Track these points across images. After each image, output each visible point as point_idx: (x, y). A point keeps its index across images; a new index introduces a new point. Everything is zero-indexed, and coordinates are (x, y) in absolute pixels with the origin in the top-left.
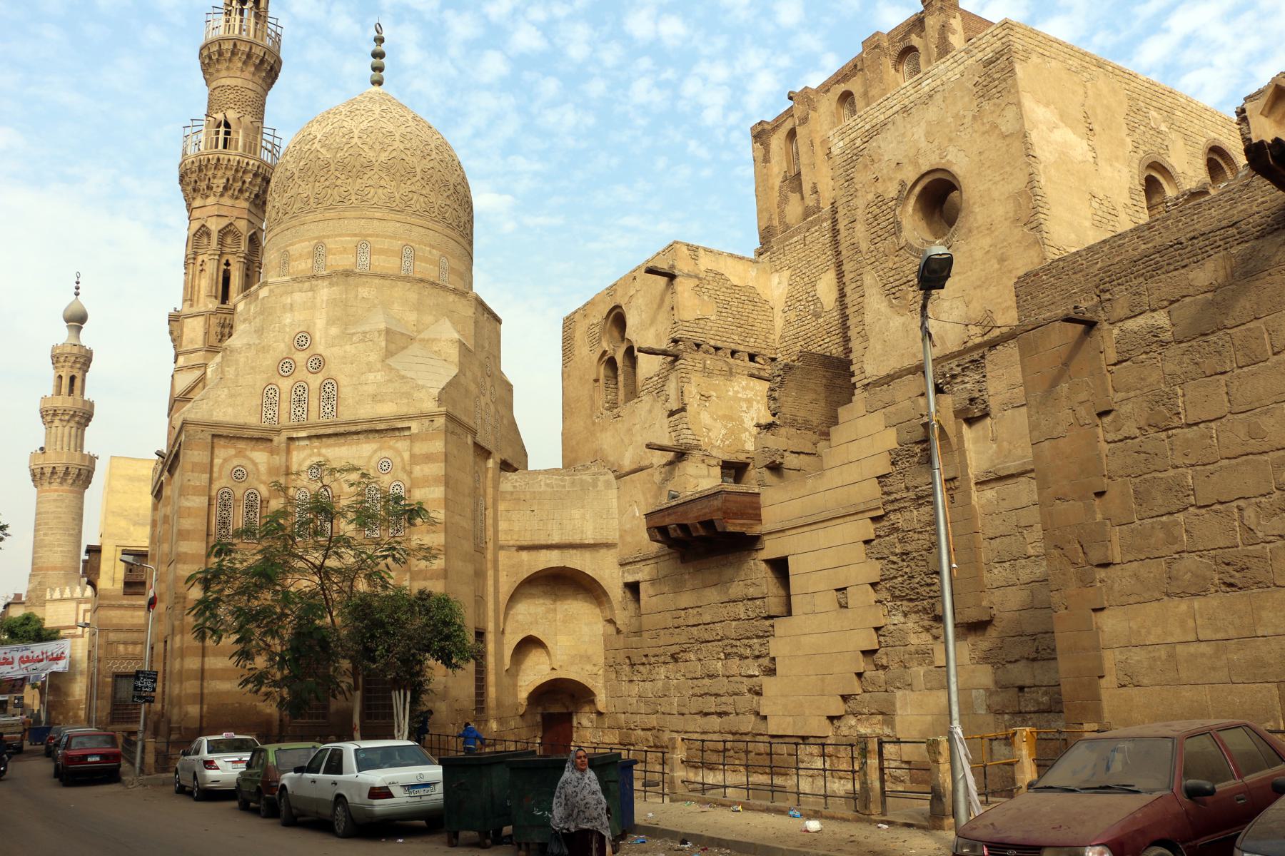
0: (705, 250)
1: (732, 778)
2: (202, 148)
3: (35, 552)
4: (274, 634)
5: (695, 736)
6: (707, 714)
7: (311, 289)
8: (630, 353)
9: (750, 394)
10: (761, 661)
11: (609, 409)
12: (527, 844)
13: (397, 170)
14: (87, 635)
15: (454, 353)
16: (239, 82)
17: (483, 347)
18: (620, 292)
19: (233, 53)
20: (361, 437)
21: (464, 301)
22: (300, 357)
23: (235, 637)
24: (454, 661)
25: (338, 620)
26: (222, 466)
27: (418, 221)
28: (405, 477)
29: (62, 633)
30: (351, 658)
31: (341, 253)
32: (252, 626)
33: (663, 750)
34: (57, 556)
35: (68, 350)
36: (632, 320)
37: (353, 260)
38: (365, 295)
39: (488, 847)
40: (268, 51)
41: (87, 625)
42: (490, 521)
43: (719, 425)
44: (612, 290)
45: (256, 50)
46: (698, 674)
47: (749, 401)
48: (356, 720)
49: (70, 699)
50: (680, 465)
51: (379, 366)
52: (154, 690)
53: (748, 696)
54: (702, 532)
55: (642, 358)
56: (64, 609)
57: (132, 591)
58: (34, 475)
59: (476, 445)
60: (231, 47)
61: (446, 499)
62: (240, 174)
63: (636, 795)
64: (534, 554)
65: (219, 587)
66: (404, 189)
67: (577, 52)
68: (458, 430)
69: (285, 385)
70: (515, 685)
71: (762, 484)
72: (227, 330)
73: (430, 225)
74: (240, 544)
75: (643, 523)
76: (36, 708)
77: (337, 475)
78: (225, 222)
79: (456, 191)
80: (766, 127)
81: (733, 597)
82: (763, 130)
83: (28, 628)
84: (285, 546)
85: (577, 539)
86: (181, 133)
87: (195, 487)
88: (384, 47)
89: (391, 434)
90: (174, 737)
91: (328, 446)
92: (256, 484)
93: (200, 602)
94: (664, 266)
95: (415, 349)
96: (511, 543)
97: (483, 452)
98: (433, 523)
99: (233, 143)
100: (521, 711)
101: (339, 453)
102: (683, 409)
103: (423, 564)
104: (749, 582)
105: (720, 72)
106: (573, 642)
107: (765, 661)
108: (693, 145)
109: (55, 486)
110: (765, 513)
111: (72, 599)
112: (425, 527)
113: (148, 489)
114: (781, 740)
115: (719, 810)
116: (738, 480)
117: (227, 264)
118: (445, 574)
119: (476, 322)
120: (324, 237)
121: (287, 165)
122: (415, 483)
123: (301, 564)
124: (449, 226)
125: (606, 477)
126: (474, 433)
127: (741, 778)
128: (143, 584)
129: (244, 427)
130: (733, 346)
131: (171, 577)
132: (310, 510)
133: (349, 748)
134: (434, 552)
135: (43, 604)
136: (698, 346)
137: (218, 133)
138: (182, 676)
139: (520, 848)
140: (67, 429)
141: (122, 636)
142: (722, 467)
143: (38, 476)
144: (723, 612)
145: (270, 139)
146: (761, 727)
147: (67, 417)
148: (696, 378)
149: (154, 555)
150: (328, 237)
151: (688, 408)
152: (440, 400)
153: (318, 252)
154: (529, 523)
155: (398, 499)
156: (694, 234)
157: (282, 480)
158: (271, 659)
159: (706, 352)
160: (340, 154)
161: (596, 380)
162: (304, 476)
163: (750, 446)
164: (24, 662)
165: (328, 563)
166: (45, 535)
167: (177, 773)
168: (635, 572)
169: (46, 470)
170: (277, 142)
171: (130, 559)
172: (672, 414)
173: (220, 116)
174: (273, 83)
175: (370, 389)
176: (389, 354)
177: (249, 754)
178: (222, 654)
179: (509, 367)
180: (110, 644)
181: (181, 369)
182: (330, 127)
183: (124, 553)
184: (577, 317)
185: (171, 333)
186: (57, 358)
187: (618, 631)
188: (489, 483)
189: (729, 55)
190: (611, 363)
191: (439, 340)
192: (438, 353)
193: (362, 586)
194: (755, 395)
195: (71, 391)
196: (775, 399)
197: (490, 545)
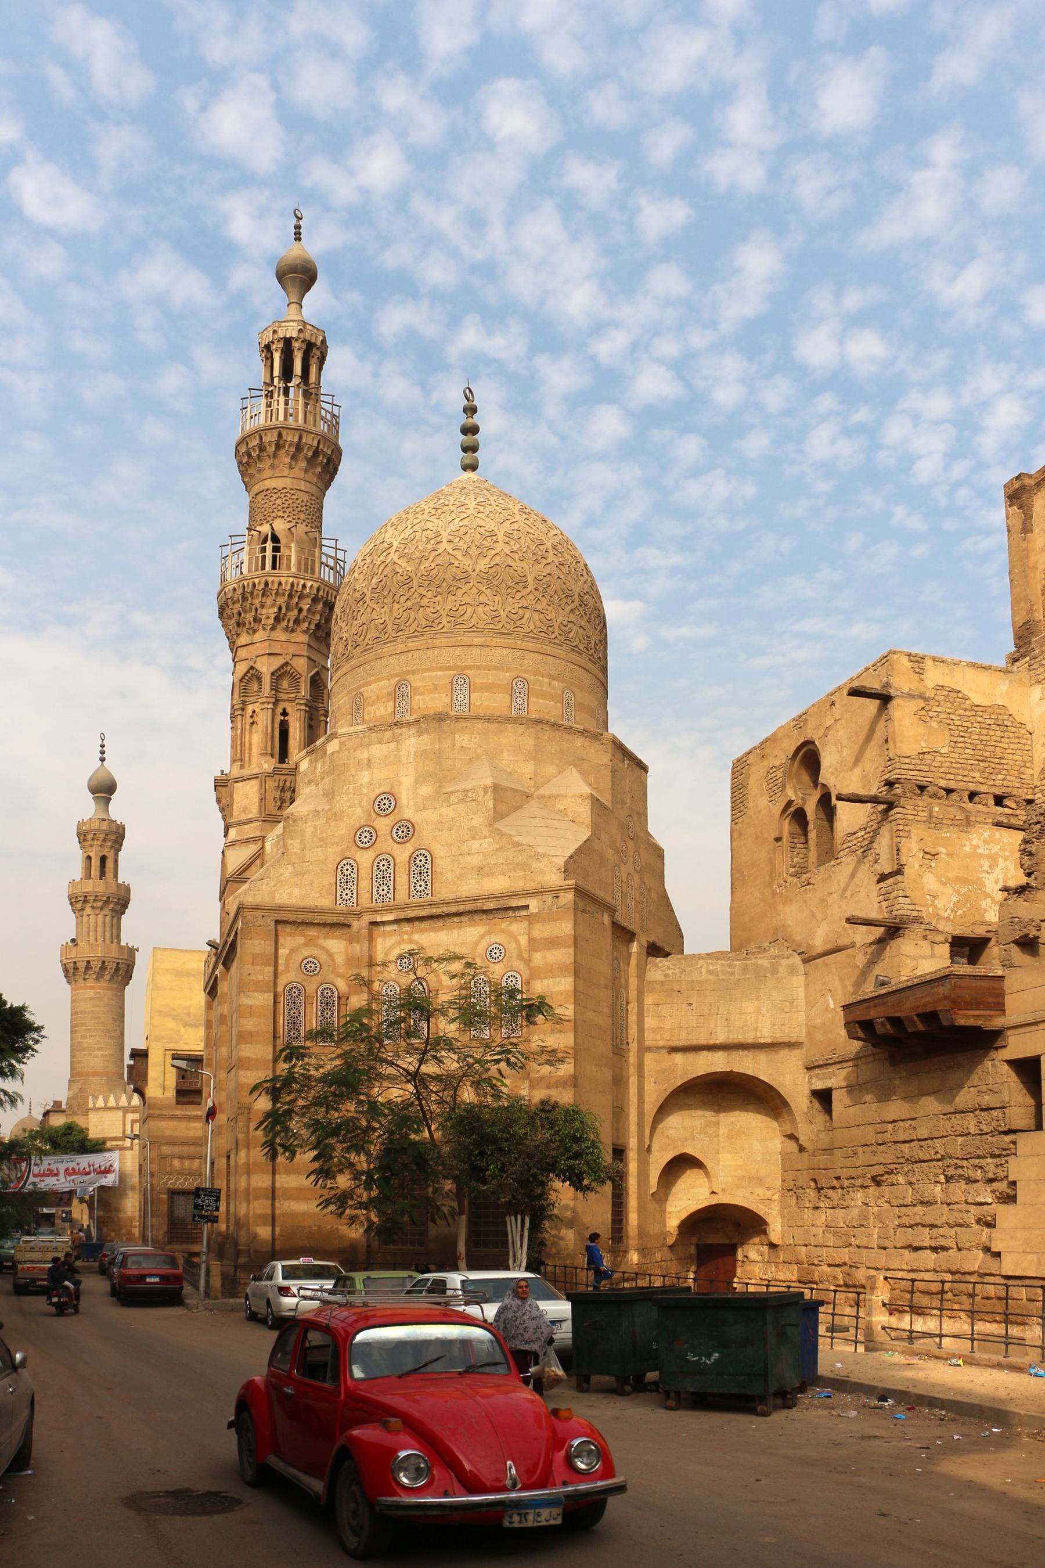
0: (934, 660)
1: (949, 1326)
2: (245, 571)
3: (72, 1056)
4: (359, 1149)
5: (900, 1275)
6: (917, 1249)
7: (394, 740)
8: (826, 803)
9: (995, 849)
10: (995, 1185)
11: (795, 875)
12: (678, 1393)
13: (502, 581)
14: (136, 1148)
15: (584, 812)
16: (287, 483)
17: (623, 803)
18: (812, 722)
19: (278, 447)
20: (464, 919)
21: (596, 745)
22: (383, 825)
23: (313, 1154)
24: (585, 1182)
25: (438, 1135)
26: (288, 958)
27: (532, 646)
28: (522, 966)
29: (109, 1145)
30: (456, 1179)
31: (430, 692)
32: (332, 1141)
33: (858, 1292)
34: (97, 1060)
35: (96, 826)
36: (828, 759)
37: (448, 700)
39: (628, 1394)
40: (323, 438)
41: (137, 1136)
42: (633, 1018)
43: (949, 890)
44: (800, 721)
45: (308, 440)
46: (908, 1201)
47: (993, 859)
48: (462, 1248)
49: (121, 1215)
50: (893, 943)
51: (486, 831)
52: (217, 1209)
53: (976, 1227)
54: (921, 1027)
55: (841, 807)
56: (108, 1119)
57: (185, 1100)
58: (66, 970)
59: (615, 925)
60: (296, 439)
61: (576, 991)
62: (295, 600)
63: (820, 1340)
64: (691, 1056)
65: (291, 1097)
66: (512, 605)
67: (727, 396)
68: (591, 908)
69: (365, 858)
70: (663, 1212)
71: (1007, 964)
72: (288, 795)
73: (549, 649)
74: (315, 1047)
75: (840, 1016)
76: (86, 1223)
77: (435, 965)
78: (278, 662)
79: (582, 603)
80: (1027, 482)
81: (960, 1107)
82: (1023, 487)
83: (71, 1138)
84: (370, 1050)
85: (749, 1038)
86: (217, 553)
87: (257, 982)
88: (477, 419)
89: (502, 914)
90: (242, 1260)
91: (422, 931)
92: (331, 977)
93: (268, 1115)
94: (876, 685)
95: (532, 808)
96: (661, 1043)
97: (624, 934)
98: (560, 1020)
99: (284, 562)
100: (670, 1241)
101: (436, 939)
102: (899, 872)
103: (546, 1069)
104: (984, 1088)
105: (939, 405)
106: (739, 1161)
107: (1003, 1186)
108: (900, 512)
109: (91, 982)
110: (1009, 1002)
111: (117, 1108)
112: (547, 1026)
113: (201, 985)
114: (1019, 1282)
115: (931, 1364)
116: (973, 960)
117: (285, 713)
118: (574, 1081)
119: (614, 772)
120: (408, 672)
121: (357, 583)
122: (535, 973)
123: (391, 1070)
124: (574, 649)
125: (790, 961)
126: (612, 911)
127: (963, 1326)
128: (199, 1092)
129: (313, 911)
130: (972, 787)
131: (232, 1085)
132: (401, 1007)
133: (455, 1279)
134: (560, 1055)
135: (86, 1112)
136: (922, 788)
137: (264, 550)
138: (249, 1195)
139: (668, 1397)
140: (100, 917)
141: (176, 1149)
142: (952, 945)
143: (71, 972)
144: (946, 1126)
145: (332, 552)
146: (992, 1266)
147: (99, 904)
148: (917, 831)
149: (209, 1060)
150: (413, 672)
151: (906, 870)
152: (566, 871)
153: (397, 695)
154: (677, 1020)
155: (512, 993)
156: (905, 636)
157: (365, 973)
158: (356, 1178)
159: (934, 796)
160: (425, 564)
161: (778, 839)
162: (392, 967)
163: (992, 916)
164: (70, 1175)
165: (425, 1069)
166: (83, 1037)
167: (247, 1298)
168: (825, 1077)
169: (79, 965)
170: (340, 555)
171: (183, 1064)
172: (883, 878)
173: (265, 529)
174: (332, 479)
175: (475, 861)
176: (498, 815)
177: (333, 1282)
178: (298, 1172)
179: (660, 825)
180: (163, 1158)
181: (233, 844)
182: (409, 531)
183: (175, 1057)
184: (751, 758)
185: (219, 801)
186: (83, 836)
187: (802, 1149)
188: (632, 971)
189: (952, 379)
190: (799, 817)
191: (565, 797)
192: (563, 812)
193: (468, 1095)
194: (1003, 849)
195: (103, 874)
196: (1031, 854)
197: (633, 1047)
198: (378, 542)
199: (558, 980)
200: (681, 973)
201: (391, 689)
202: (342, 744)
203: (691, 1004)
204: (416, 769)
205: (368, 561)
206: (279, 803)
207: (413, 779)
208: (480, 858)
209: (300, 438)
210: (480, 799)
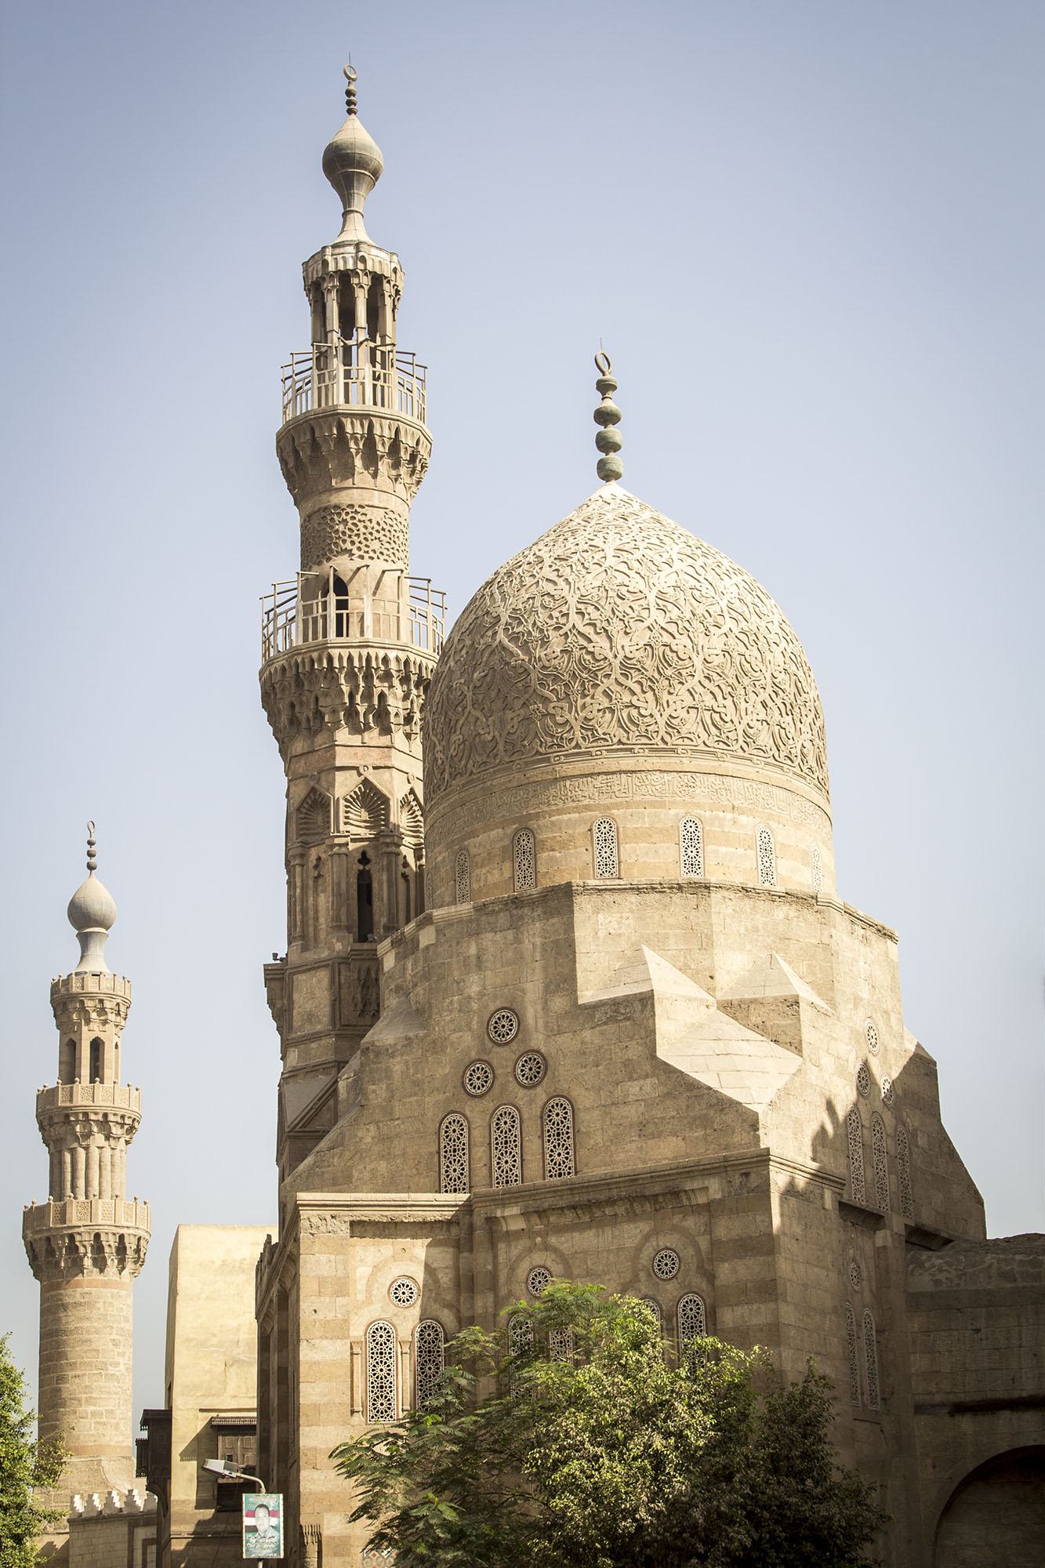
22: (503, 1058)
26: (371, 1281)
38: (613, 927)
64: (985, 1421)
69: (477, 1113)
96: (938, 1398)
99: (354, 620)
175: (633, 1113)
198: (480, 613)
199: (755, 1307)
200: (959, 1277)
201: (507, 842)
202: (439, 932)
203: (977, 1331)
204: (545, 969)
205: (468, 642)
206: (360, 1006)
207: (541, 986)
208: (642, 1108)
209: (371, 426)
210: (637, 1015)
